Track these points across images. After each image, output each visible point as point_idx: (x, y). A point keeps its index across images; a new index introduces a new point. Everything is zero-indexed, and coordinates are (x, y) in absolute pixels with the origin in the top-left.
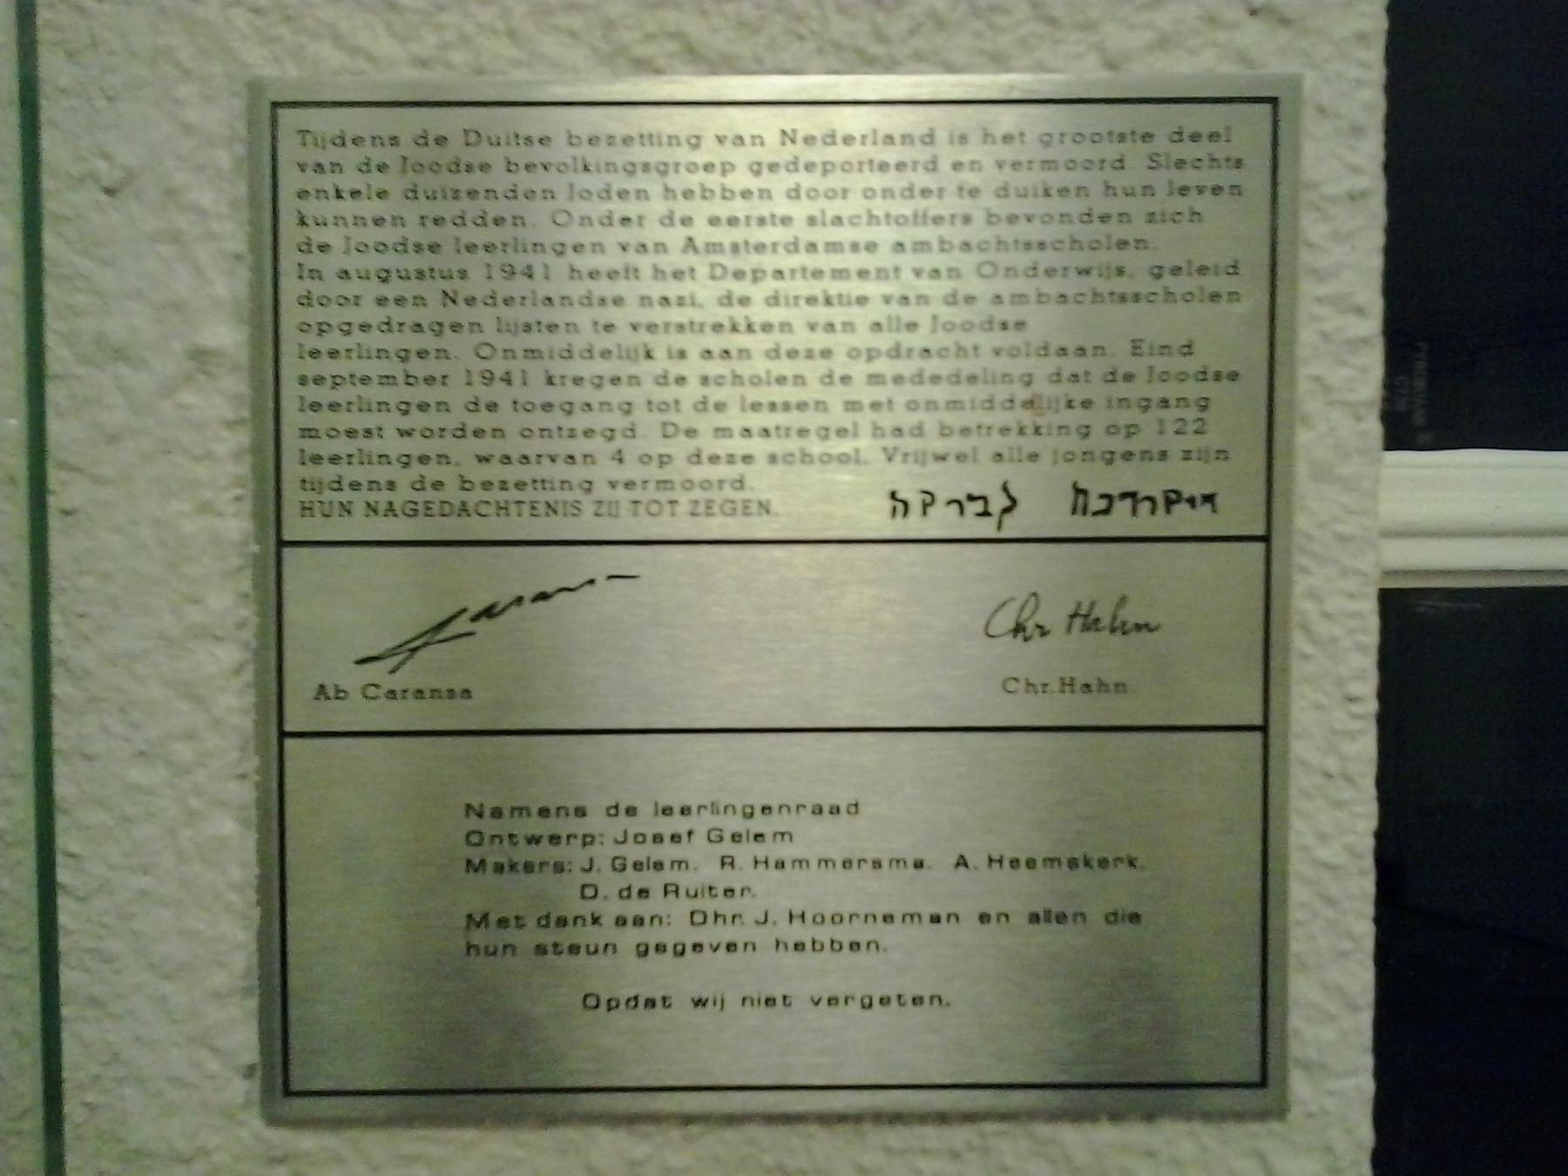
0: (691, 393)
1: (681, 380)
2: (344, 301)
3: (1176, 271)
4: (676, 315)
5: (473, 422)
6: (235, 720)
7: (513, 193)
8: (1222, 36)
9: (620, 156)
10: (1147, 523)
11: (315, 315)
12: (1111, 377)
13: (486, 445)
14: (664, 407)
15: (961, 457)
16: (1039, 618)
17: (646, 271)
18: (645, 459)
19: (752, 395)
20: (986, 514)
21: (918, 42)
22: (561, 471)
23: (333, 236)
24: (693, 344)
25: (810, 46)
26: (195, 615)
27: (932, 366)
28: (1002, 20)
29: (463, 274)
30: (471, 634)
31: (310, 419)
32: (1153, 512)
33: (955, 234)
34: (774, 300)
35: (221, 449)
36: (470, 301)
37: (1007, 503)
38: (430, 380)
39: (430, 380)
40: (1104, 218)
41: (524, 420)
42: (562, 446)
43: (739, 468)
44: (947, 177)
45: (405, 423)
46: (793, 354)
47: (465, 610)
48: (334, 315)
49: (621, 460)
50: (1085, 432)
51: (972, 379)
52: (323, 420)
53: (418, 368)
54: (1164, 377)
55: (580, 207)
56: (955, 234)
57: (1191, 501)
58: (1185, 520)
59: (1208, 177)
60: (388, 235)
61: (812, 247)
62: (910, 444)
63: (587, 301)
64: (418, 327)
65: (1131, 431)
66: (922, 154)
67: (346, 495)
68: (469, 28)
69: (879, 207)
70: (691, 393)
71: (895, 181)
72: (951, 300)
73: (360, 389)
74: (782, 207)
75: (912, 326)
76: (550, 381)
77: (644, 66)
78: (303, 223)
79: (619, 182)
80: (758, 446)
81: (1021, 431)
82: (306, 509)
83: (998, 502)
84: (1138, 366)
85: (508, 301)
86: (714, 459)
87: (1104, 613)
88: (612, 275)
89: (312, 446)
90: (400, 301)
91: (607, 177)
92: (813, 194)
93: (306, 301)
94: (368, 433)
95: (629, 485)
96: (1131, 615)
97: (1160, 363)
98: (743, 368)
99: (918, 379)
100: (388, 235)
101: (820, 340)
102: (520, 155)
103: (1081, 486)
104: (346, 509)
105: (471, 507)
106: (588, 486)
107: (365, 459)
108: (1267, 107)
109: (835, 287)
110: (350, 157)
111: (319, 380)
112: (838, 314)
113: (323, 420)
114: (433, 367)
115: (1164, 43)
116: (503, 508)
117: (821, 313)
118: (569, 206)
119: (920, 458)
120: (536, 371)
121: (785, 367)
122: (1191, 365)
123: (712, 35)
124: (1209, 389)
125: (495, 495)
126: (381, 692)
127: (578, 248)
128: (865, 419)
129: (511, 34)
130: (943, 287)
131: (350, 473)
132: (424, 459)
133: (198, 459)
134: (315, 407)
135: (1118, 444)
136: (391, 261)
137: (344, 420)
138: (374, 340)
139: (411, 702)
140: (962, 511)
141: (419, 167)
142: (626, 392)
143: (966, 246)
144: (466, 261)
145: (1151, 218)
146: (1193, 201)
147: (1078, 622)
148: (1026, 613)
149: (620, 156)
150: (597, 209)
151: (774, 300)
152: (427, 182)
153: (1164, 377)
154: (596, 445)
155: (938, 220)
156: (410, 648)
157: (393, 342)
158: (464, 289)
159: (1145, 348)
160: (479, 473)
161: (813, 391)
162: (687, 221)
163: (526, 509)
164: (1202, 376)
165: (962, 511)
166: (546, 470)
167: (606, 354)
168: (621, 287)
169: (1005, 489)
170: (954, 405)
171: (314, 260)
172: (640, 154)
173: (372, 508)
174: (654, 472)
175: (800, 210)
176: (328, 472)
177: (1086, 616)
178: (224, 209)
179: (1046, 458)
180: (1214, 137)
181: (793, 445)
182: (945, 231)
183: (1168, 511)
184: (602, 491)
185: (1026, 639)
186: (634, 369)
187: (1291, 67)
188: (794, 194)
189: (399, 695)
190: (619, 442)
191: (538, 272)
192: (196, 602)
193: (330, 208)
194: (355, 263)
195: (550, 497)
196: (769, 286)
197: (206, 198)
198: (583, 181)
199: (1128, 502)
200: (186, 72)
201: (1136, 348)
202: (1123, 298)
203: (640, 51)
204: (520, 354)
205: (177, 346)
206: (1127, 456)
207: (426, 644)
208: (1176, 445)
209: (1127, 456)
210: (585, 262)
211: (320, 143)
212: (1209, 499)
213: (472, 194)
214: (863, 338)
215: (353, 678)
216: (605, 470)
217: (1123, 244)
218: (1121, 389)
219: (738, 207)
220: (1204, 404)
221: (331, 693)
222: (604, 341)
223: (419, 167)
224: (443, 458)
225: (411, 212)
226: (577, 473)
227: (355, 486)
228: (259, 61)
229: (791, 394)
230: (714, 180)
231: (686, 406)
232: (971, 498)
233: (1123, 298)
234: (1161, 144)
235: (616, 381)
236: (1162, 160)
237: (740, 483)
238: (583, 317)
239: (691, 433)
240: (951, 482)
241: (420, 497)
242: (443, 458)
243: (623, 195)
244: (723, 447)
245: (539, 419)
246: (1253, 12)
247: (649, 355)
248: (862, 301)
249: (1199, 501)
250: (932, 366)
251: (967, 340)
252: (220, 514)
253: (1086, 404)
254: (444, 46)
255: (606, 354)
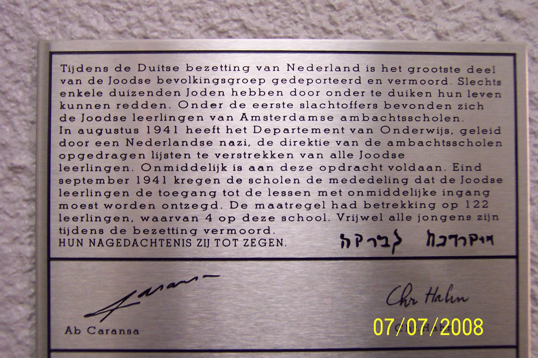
0: (245, 186)
1: (239, 181)
2: (80, 144)
3: (472, 131)
4: (236, 150)
5: (140, 201)
6: (28, 342)
7: (160, 93)
8: (488, 25)
9: (212, 75)
10: (462, 250)
11: (67, 150)
12: (444, 180)
13: (146, 212)
14: (231, 194)
15: (374, 218)
16: (412, 295)
17: (223, 130)
18: (222, 219)
19: (274, 188)
20: (387, 245)
21: (351, 25)
22: (181, 225)
23: (77, 113)
24: (246, 163)
25: (301, 26)
26: (10, 291)
27: (360, 175)
28: (390, 17)
29: (136, 131)
30: (139, 303)
31: (64, 200)
32: (465, 244)
33: (370, 113)
34: (284, 143)
35: (23, 213)
36: (139, 144)
37: (397, 240)
38: (120, 181)
39: (120, 181)
40: (439, 107)
41: (164, 200)
42: (182, 213)
43: (268, 223)
44: (368, 89)
45: (108, 202)
46: (293, 168)
47: (136, 291)
48: (76, 150)
49: (210, 219)
50: (433, 206)
51: (379, 181)
52: (70, 200)
53: (114, 175)
54: (468, 181)
55: (191, 100)
56: (370, 113)
57: (482, 239)
58: (479, 248)
59: (486, 89)
60: (103, 113)
61: (303, 118)
62: (349, 212)
63: (195, 143)
64: (115, 156)
65: (454, 206)
66: (354, 76)
67: (80, 236)
68: (142, 17)
69: (334, 100)
70: (245, 186)
71: (343, 88)
72: (369, 143)
73: (87, 186)
74: (288, 99)
75: (350, 156)
76: (176, 181)
77: (222, 34)
78: (62, 107)
79: (211, 87)
80: (278, 213)
81: (403, 206)
82: (62, 242)
83: (393, 240)
84: (457, 175)
85: (157, 143)
86: (255, 219)
87: (442, 293)
88: (207, 131)
89: (65, 213)
90: (106, 144)
91: (206, 85)
92: (303, 93)
93: (63, 143)
94: (91, 206)
95: (214, 231)
96: (454, 293)
97: (467, 174)
98: (270, 175)
99: (354, 180)
100: (103, 113)
101: (306, 162)
102: (165, 75)
103: (431, 232)
104: (80, 243)
105: (138, 242)
106: (195, 232)
107: (89, 219)
108: (511, 58)
109: (313, 137)
110: (85, 76)
111: (68, 181)
112: (314, 150)
113: (70, 200)
114: (121, 175)
115: (463, 28)
116: (153, 243)
117: (307, 149)
118: (186, 99)
119: (355, 219)
120: (170, 176)
121: (289, 174)
122: (481, 175)
123: (258, 21)
124: (488, 186)
125: (150, 236)
126: (97, 331)
127: (191, 118)
128: (329, 199)
129: (161, 20)
130: (366, 137)
131: (82, 225)
132: (116, 219)
133: (12, 217)
134: (66, 194)
135: (448, 212)
136: (103, 125)
137: (79, 200)
138: (95, 162)
139: (110, 335)
140: (375, 245)
141: (116, 82)
142: (213, 187)
143: (375, 118)
144: (137, 124)
145: (460, 107)
146: (479, 99)
147: (431, 297)
148: (406, 293)
149: (212, 75)
150: (200, 100)
151: (284, 143)
152: (120, 88)
153: (468, 181)
154: (198, 212)
155: (362, 106)
156: (110, 310)
157: (103, 163)
158: (137, 138)
159: (459, 167)
160: (143, 225)
161: (303, 186)
162: (242, 106)
163: (165, 243)
164: (486, 180)
165: (375, 245)
166: (174, 224)
167: (203, 168)
168: (210, 137)
169: (396, 233)
170: (370, 193)
171: (67, 125)
172: (220, 74)
173: (92, 242)
174: (225, 225)
175: (296, 101)
176: (72, 225)
177: (434, 294)
178: (27, 101)
179: (415, 219)
180: (487, 71)
181: (294, 212)
182: (365, 111)
183: (471, 244)
184: (201, 234)
185: (406, 306)
186: (217, 176)
187: (521, 40)
188: (294, 93)
189: (105, 332)
190: (209, 210)
191: (172, 130)
192: (11, 285)
193: (76, 100)
194: (86, 125)
195: (177, 237)
196: (282, 136)
197: (19, 95)
198: (193, 87)
199: (453, 240)
200: (12, 38)
201: (455, 166)
202: (449, 144)
203: (222, 27)
204: (162, 169)
205: (4, 164)
206: (452, 218)
207: (117, 308)
208: (474, 213)
209: (452, 218)
210: (194, 125)
211: (72, 70)
212: (490, 238)
213: (141, 93)
214: (327, 162)
215: (84, 324)
216: (202, 225)
217: (447, 119)
218: (448, 186)
219: (267, 99)
220: (487, 194)
221: (73, 330)
222: (202, 162)
223: (116, 82)
224: (126, 219)
225: (113, 102)
226: (190, 226)
227: (84, 231)
228: (44, 32)
229: (293, 188)
230: (255, 87)
231: (242, 193)
232: (379, 238)
233: (449, 144)
234: (463, 73)
235: (208, 181)
236: (465, 80)
237: (268, 230)
238: (193, 150)
239: (244, 206)
240: (368, 230)
241: (115, 237)
242: (126, 219)
243: (212, 93)
244: (260, 213)
245: (171, 200)
246: (502, 15)
247: (224, 169)
248: (326, 143)
249: (485, 239)
250: (360, 175)
251: (377, 163)
252: (22, 244)
253: (433, 193)
254: (129, 26)
255: (203, 168)
